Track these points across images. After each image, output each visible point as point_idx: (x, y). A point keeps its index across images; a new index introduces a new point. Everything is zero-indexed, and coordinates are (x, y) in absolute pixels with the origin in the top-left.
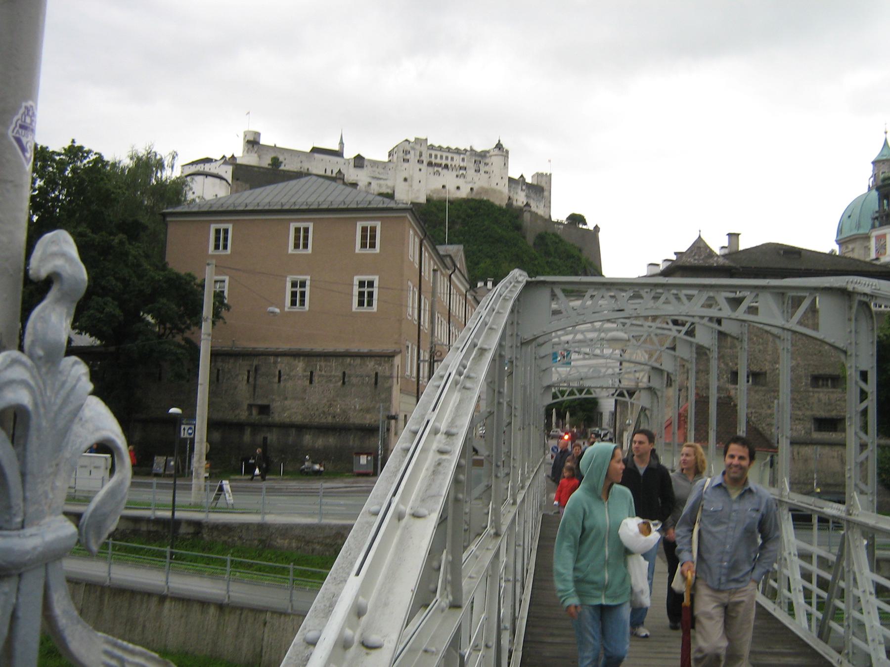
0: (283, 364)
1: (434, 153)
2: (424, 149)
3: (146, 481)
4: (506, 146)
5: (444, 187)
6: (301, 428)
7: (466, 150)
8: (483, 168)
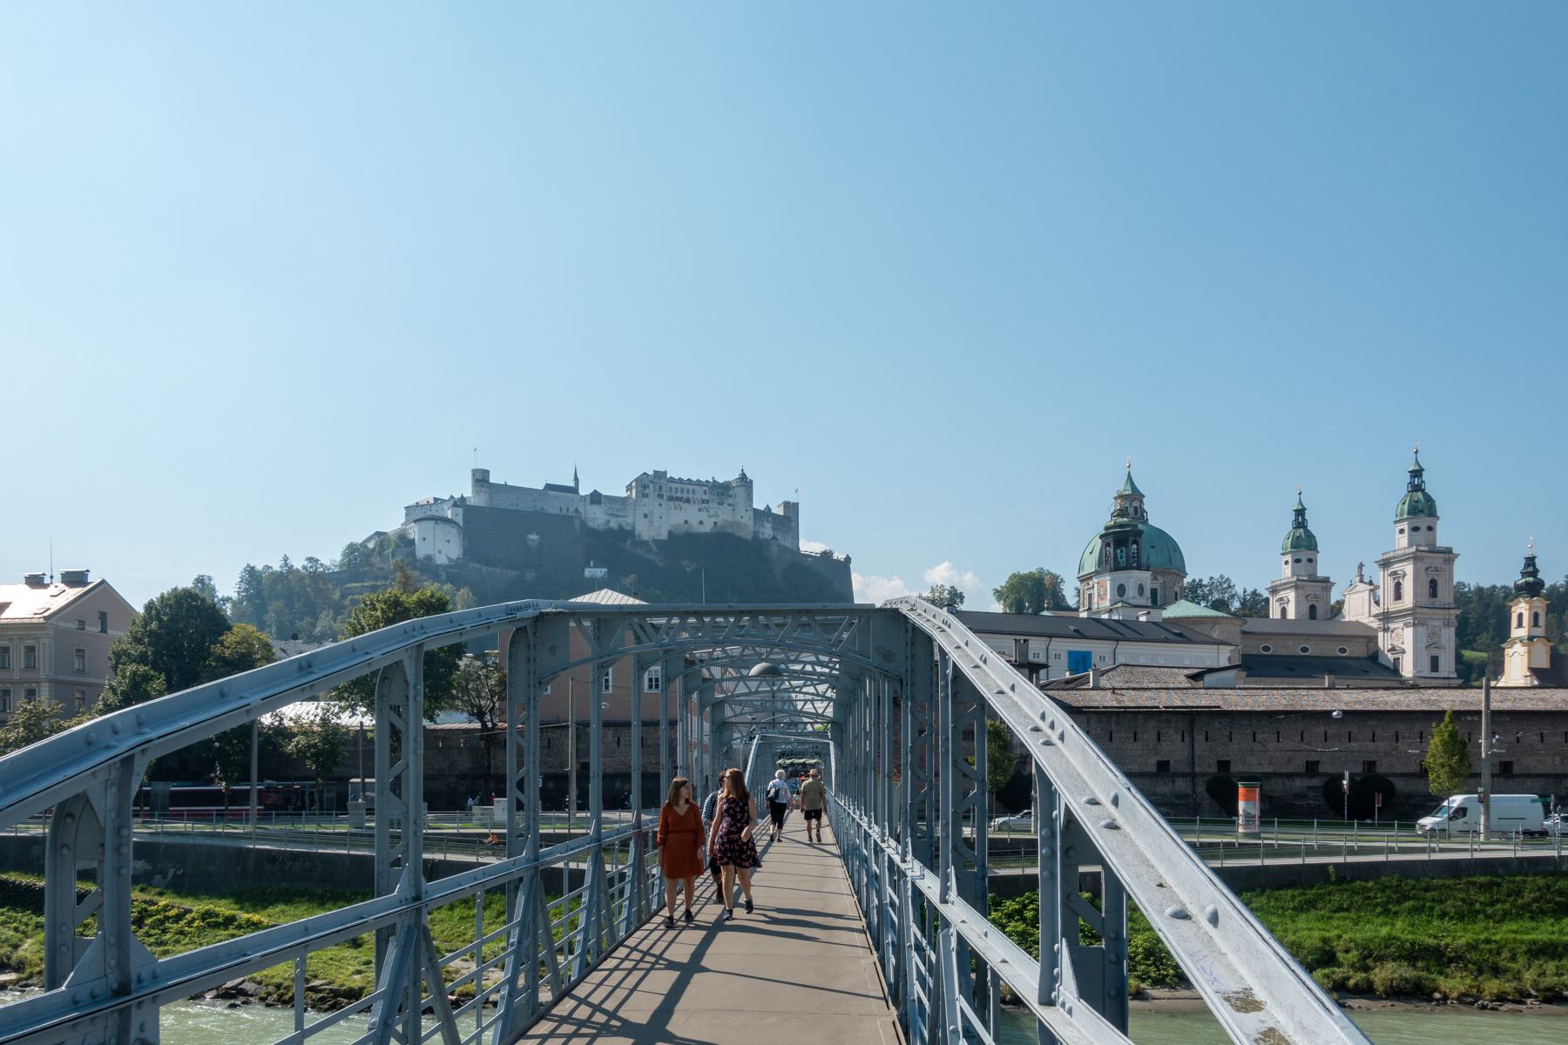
4: (749, 476)
5: (686, 522)
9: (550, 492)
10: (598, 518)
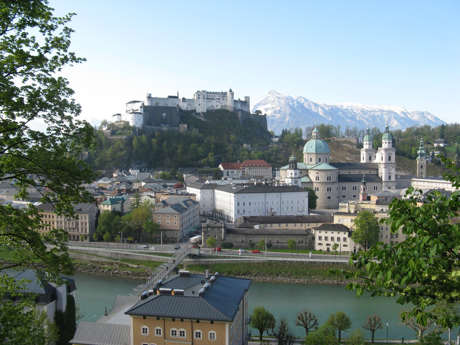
0: (167, 231)
1: (208, 95)
2: (205, 94)
4: (233, 91)
5: (212, 106)
6: (169, 238)
7: (219, 93)
8: (225, 98)
9: (170, 99)
10: (184, 106)
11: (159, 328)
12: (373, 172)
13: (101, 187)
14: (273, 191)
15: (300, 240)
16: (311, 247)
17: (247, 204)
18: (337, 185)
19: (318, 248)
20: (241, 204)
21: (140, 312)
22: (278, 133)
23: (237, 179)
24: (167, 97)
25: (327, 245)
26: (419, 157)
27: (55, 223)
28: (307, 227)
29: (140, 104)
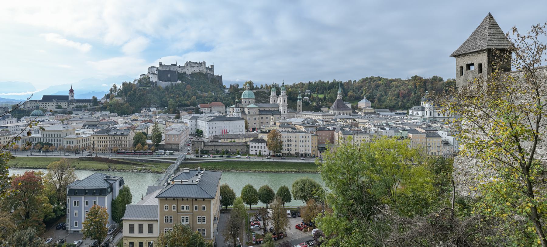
3: (133, 158)
4: (205, 62)
10: (180, 70)
11: (174, 205)
12: (276, 109)
13: (134, 119)
14: (227, 120)
15: (242, 148)
16: (247, 153)
17: (214, 128)
18: (258, 116)
19: (251, 153)
20: (211, 128)
21: (164, 196)
22: (228, 87)
23: (208, 113)
24: (41, 99)
25: (256, 151)
26: (298, 100)
27: (108, 142)
28: (245, 141)
29: (155, 69)
